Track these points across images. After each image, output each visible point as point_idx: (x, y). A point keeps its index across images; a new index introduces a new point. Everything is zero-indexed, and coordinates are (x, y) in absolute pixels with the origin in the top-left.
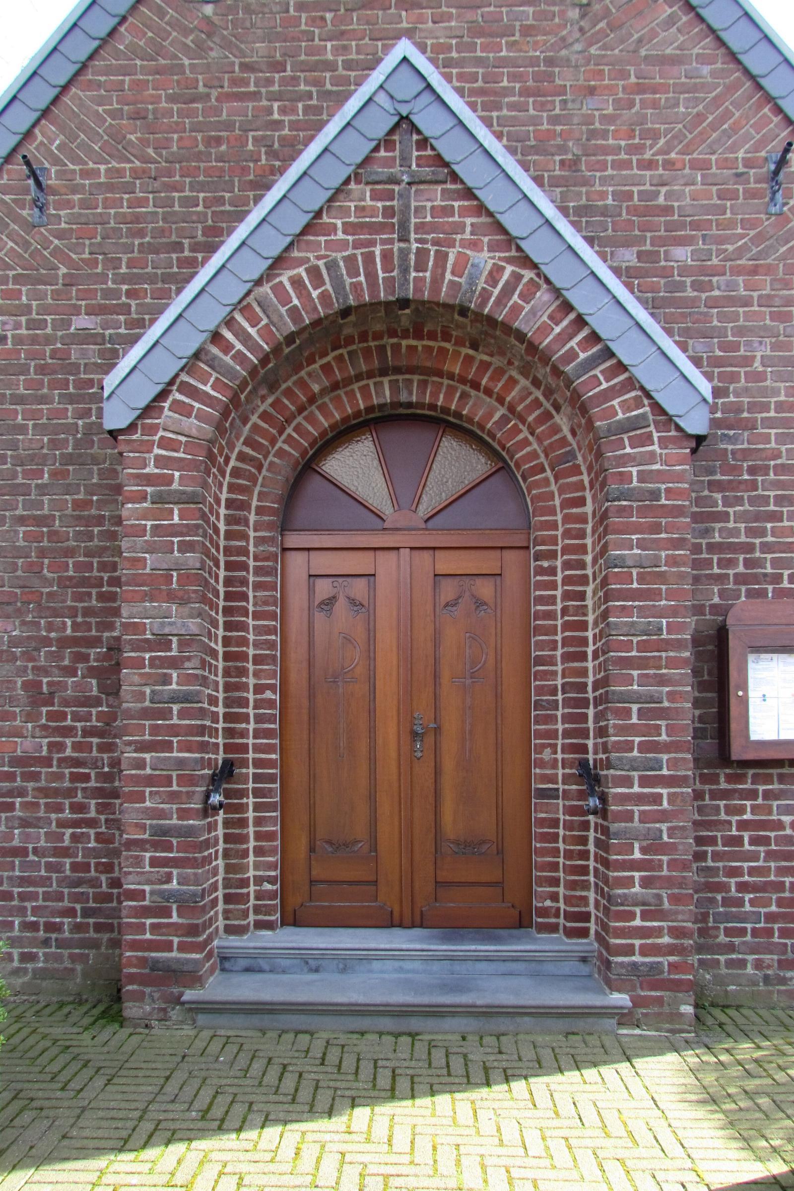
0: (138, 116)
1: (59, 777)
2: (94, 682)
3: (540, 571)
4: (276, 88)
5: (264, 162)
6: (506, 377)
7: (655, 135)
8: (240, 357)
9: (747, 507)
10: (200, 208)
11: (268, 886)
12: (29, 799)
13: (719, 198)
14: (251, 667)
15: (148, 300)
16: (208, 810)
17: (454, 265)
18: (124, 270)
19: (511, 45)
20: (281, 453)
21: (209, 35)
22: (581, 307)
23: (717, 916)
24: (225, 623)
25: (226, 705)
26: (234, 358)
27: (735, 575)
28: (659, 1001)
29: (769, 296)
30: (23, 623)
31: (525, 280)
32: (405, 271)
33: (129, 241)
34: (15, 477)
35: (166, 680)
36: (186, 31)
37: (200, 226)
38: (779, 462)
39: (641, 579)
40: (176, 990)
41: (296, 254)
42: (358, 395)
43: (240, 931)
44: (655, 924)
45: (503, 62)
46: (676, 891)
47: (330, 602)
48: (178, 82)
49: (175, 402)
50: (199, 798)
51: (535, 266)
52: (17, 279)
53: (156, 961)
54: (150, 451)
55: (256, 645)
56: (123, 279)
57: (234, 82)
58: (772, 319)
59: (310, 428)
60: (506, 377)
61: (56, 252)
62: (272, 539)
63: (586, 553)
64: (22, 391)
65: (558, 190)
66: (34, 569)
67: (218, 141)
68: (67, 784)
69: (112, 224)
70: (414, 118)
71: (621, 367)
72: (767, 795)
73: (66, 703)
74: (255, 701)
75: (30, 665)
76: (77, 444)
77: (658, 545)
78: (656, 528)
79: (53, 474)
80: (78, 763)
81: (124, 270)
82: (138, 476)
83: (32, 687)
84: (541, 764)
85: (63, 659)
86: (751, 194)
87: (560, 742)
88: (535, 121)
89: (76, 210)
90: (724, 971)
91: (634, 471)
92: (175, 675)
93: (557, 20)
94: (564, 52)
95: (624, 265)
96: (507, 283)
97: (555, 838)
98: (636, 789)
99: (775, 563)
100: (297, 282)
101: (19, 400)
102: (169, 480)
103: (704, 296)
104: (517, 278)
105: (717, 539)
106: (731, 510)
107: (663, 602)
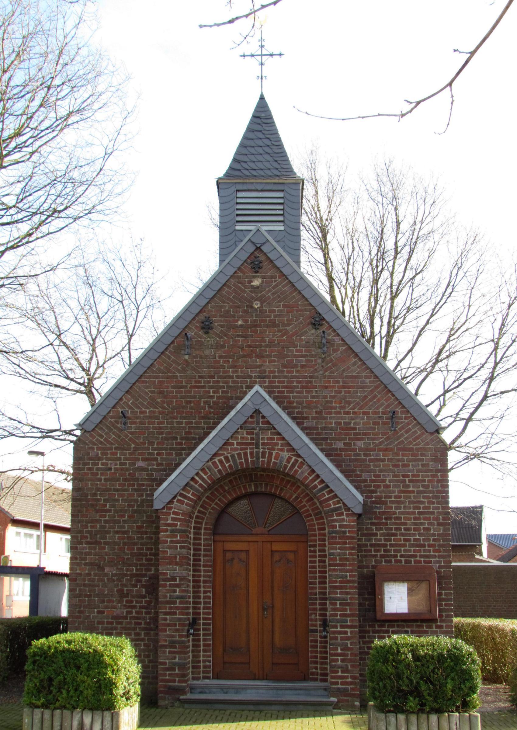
0: (161, 393)
1: (130, 623)
2: (144, 590)
3: (311, 551)
4: (211, 384)
5: (207, 410)
6: (296, 485)
7: (349, 403)
8: (200, 485)
9: (384, 531)
10: (184, 425)
11: (208, 664)
12: (119, 631)
13: (373, 425)
14: (202, 584)
15: (164, 456)
16: (188, 635)
17: (275, 456)
18: (155, 446)
19: (297, 371)
20: (213, 509)
21: (187, 366)
22: (318, 472)
24: (193, 570)
25: (193, 598)
26: (199, 485)
27: (380, 555)
28: (347, 701)
29: (391, 459)
30: (117, 569)
31: (299, 462)
32: (258, 458)
33: (157, 436)
34: (115, 517)
35: (175, 591)
36: (179, 364)
37: (184, 431)
38: (396, 516)
39: (340, 560)
40: (177, 696)
42: (242, 489)
43: (198, 679)
44: (346, 674)
46: (353, 663)
47: (232, 559)
48: (175, 381)
49: (178, 500)
50: (186, 631)
51: (302, 458)
52: (116, 448)
53: (170, 686)
54: (170, 515)
55: (204, 576)
56: (155, 449)
57: (196, 382)
58: (393, 467)
59: (224, 500)
60: (296, 485)
61: (131, 439)
62: (210, 539)
63: (326, 546)
64: (117, 487)
65: (315, 421)
66: (122, 549)
67: (190, 402)
68: (133, 626)
69: (151, 430)
70: (261, 410)
71: (331, 491)
73: (133, 597)
74: (204, 596)
75: (120, 583)
76: (138, 506)
77: (345, 549)
78: (345, 543)
79: (129, 516)
80: (137, 618)
81: (155, 446)
82: (165, 524)
83: (121, 591)
84: (311, 620)
85: (132, 581)
86: (384, 424)
87: (318, 612)
88: (306, 397)
89: (138, 425)
91: (337, 524)
92: (178, 590)
93: (313, 363)
94: (316, 374)
95: (339, 447)
96: (293, 463)
97: (316, 646)
98: (339, 629)
99: (395, 551)
100: (221, 461)
101: (117, 490)
102: (176, 525)
103: (368, 458)
104: (296, 461)
105: (374, 542)
106: (378, 532)
107: (348, 568)
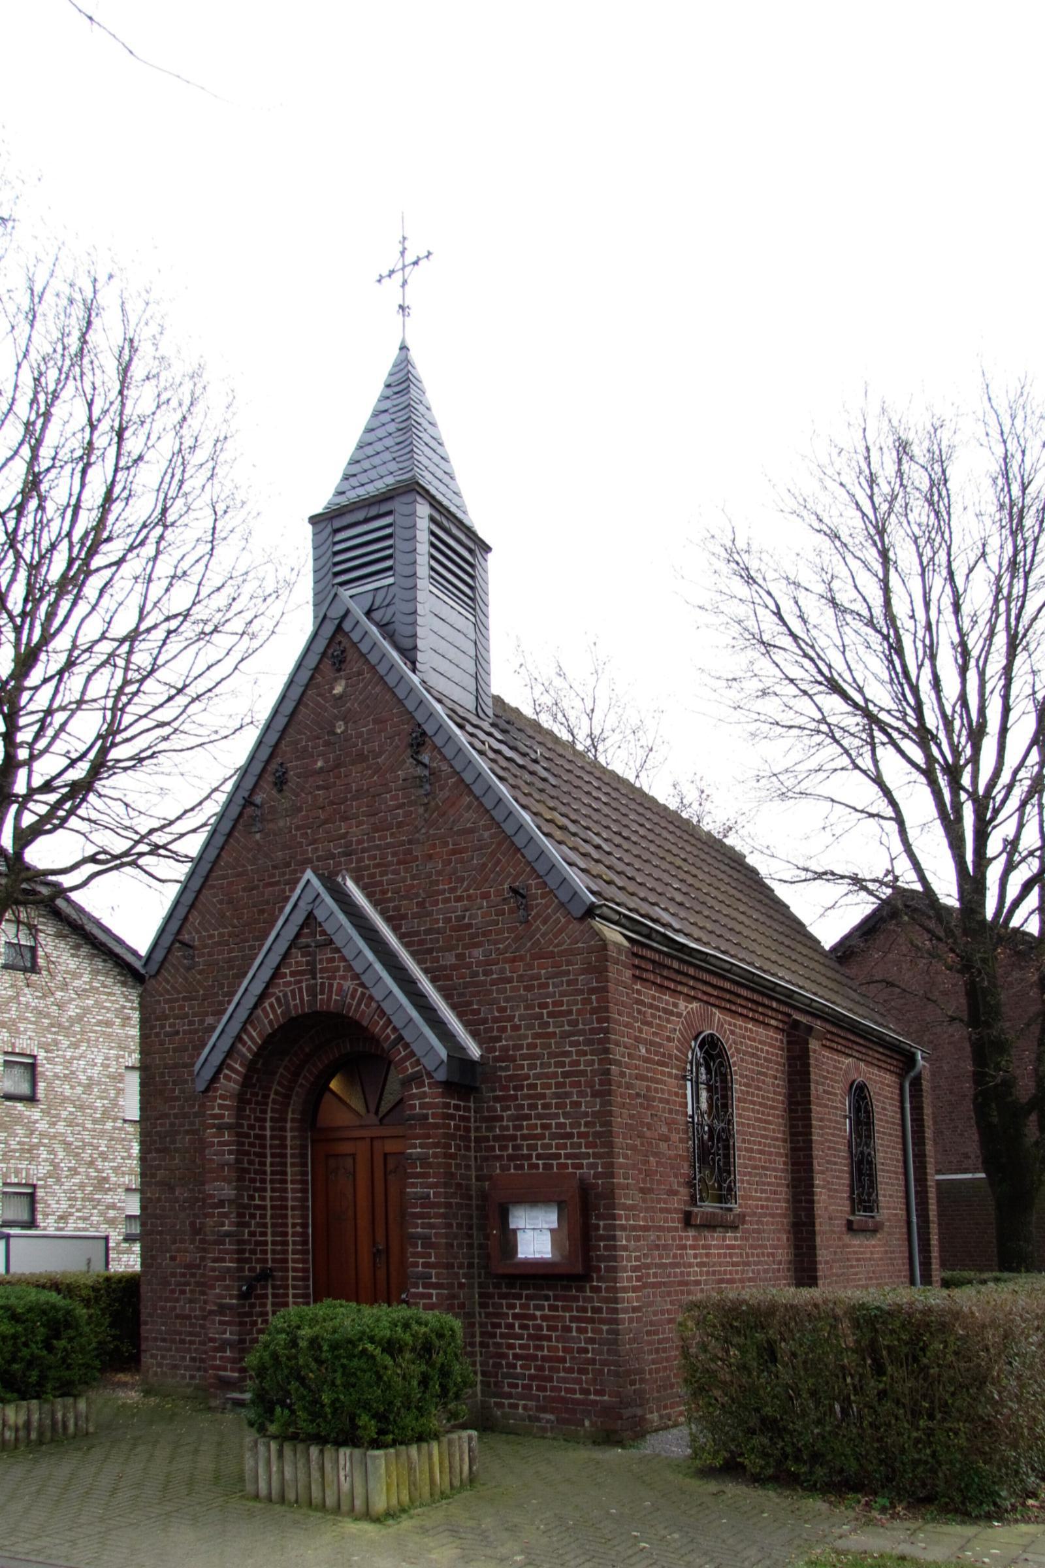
23: (503, 1373)
25: (273, 1236)
41: (271, 990)
45: (388, 846)
72: (529, 1298)
88: (404, 880)
90: (507, 1410)
91: (417, 1102)
98: (421, 1290)
